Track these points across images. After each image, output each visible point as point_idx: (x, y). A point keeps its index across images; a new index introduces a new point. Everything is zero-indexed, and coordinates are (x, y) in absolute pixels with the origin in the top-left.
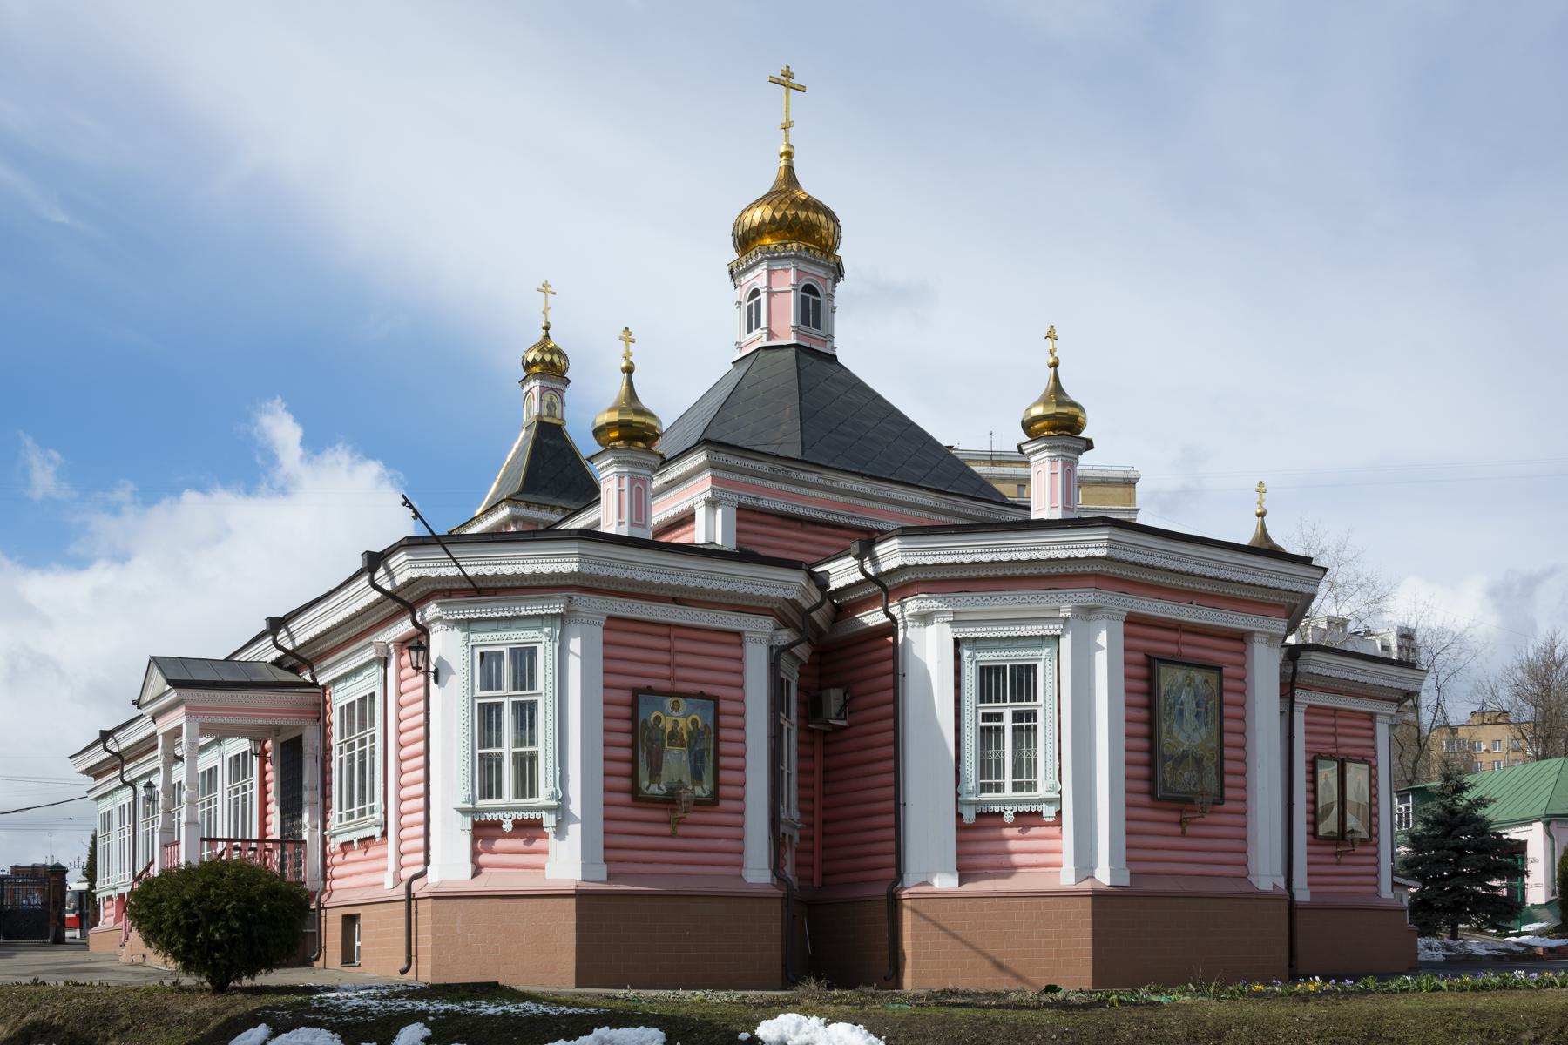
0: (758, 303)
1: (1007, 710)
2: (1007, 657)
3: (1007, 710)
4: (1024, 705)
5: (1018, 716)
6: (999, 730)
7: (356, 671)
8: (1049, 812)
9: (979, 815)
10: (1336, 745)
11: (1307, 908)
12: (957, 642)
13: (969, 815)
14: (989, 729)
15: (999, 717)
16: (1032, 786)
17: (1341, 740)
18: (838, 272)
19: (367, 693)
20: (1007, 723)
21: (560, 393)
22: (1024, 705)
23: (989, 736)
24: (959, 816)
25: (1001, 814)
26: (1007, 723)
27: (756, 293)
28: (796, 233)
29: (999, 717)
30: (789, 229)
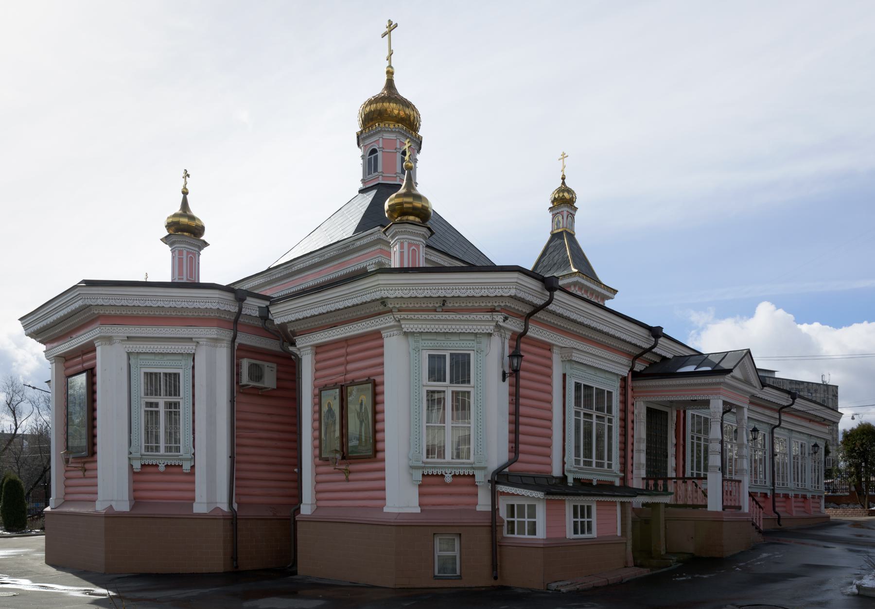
0: (376, 158)
1: (162, 401)
2: (162, 368)
3: (162, 401)
4: (173, 399)
5: (169, 405)
6: (157, 413)
7: (561, 316)
8: (186, 467)
9: (143, 466)
10: (347, 372)
11: (308, 520)
12: (129, 354)
13: (137, 465)
14: (152, 412)
15: (157, 405)
16: (178, 449)
17: (350, 367)
18: (418, 143)
19: (144, 408)
20: (162, 409)
21: (573, 216)
22: (173, 399)
23: (152, 415)
24: (131, 466)
26: (162, 409)
27: (374, 151)
28: (389, 121)
29: (157, 405)
30: (372, 120)
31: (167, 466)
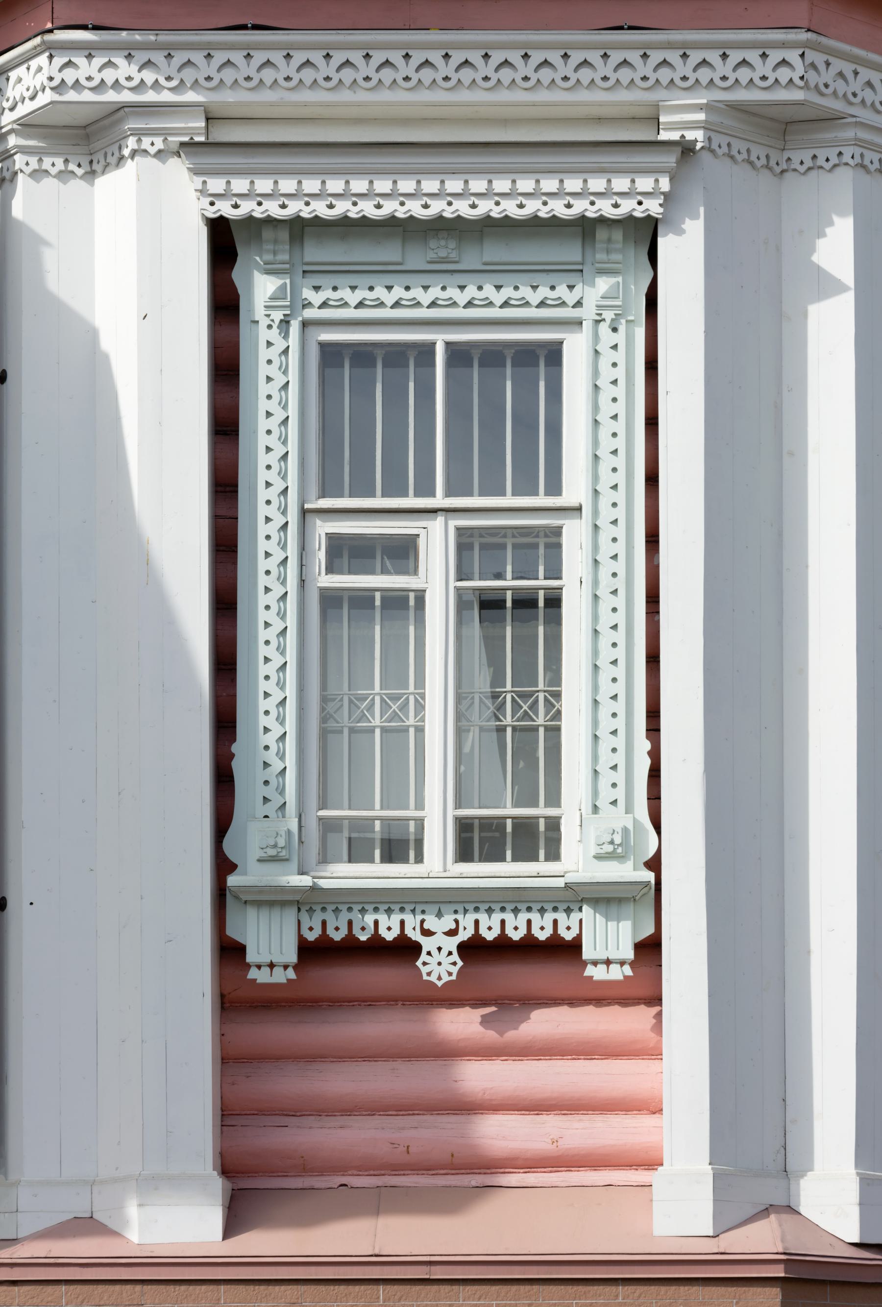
9: (312, 952)
25: (406, 950)
31: (473, 950)
